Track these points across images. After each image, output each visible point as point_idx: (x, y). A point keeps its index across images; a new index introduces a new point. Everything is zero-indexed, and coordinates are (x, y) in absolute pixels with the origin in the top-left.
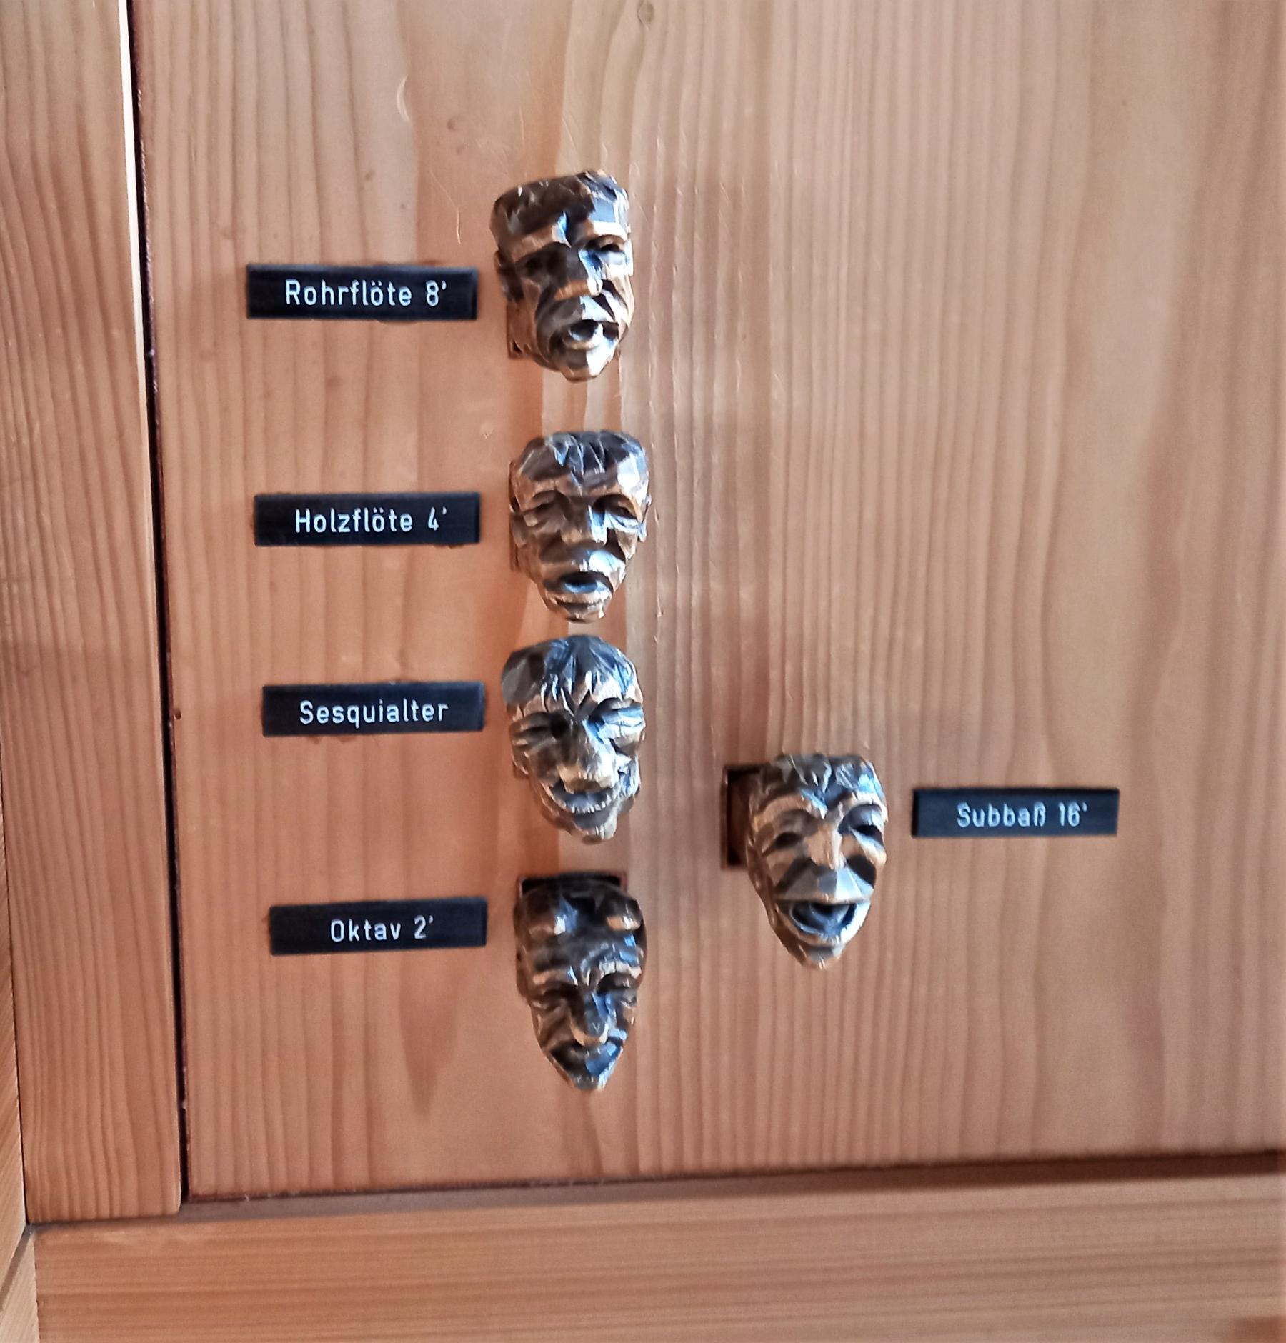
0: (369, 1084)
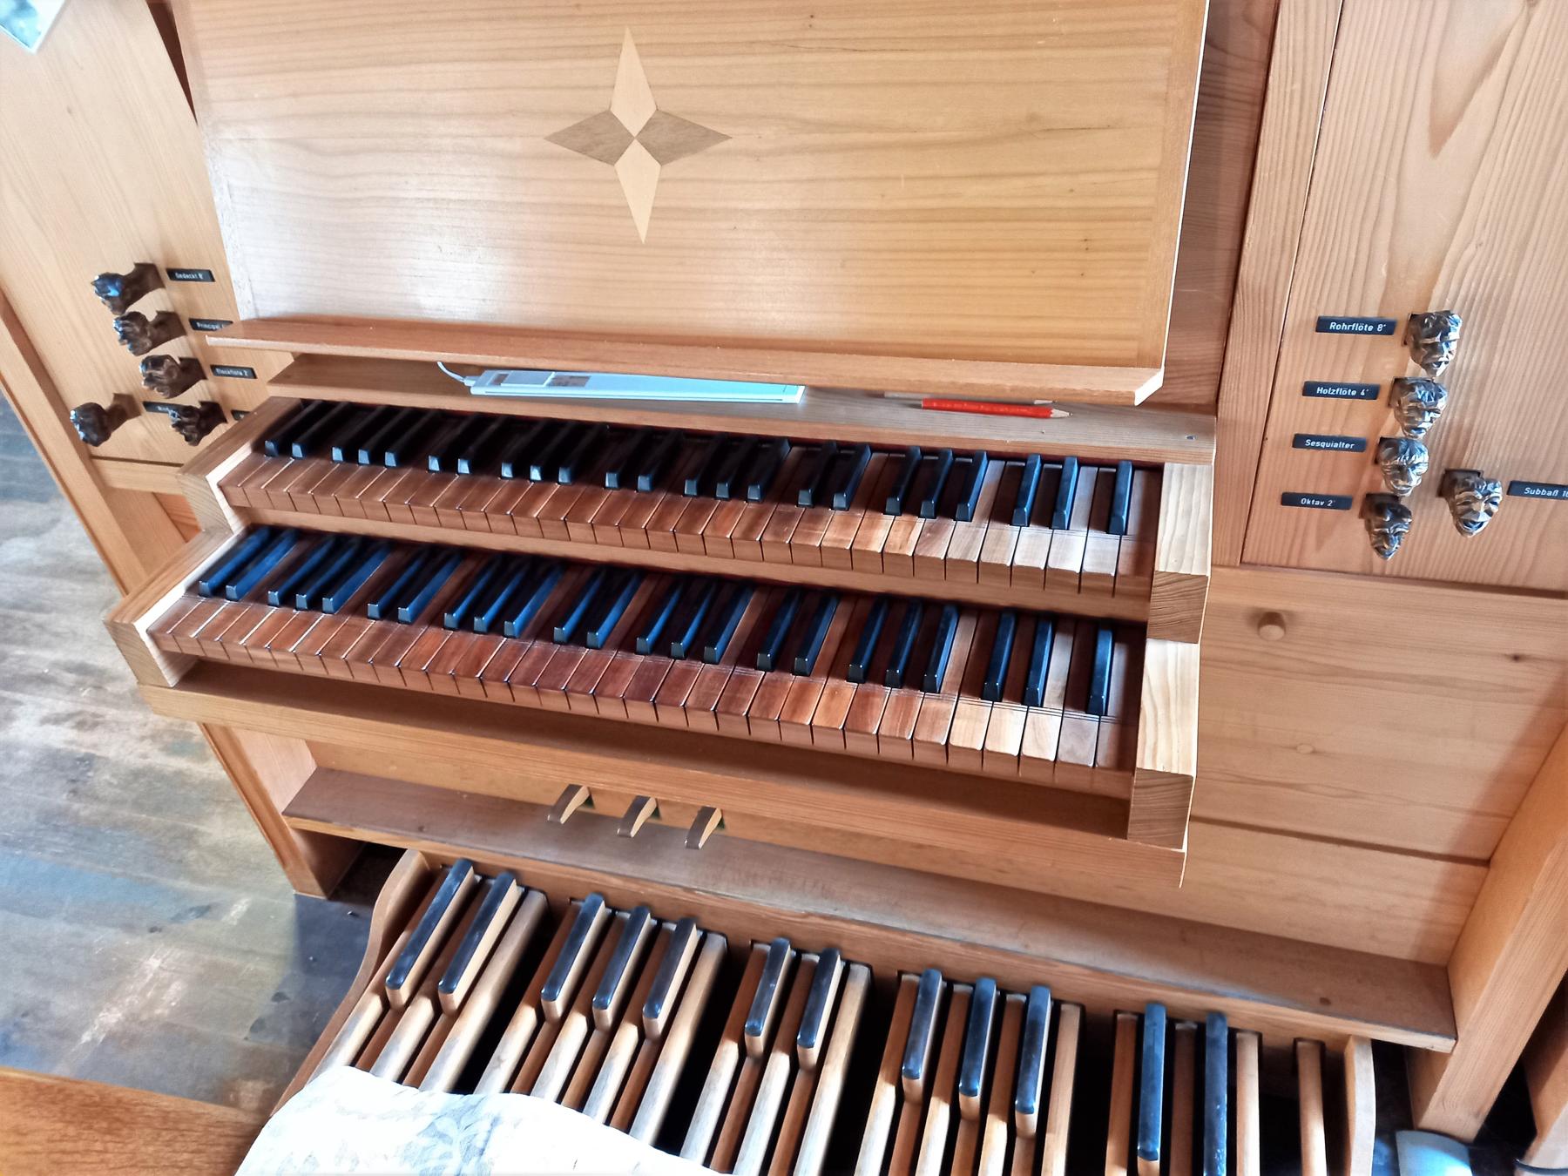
0: (1303, 541)
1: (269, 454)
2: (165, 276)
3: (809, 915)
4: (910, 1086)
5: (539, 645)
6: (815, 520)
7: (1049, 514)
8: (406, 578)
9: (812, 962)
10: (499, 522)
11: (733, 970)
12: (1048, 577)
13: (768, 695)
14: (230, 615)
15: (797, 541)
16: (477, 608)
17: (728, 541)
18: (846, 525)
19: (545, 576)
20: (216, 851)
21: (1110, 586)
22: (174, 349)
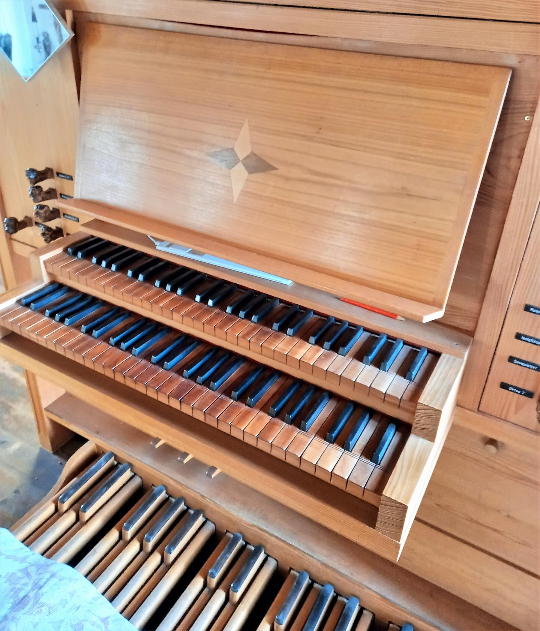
1: (69, 254)
2: (55, 175)
3: (253, 526)
4: (277, 627)
5: (144, 362)
6: (277, 337)
7: (379, 362)
8: (101, 317)
9: (251, 550)
10: (146, 304)
11: (214, 541)
12: (371, 391)
13: (232, 410)
14: (28, 315)
15: (265, 345)
16: (124, 339)
17: (237, 336)
18: (289, 343)
19: (159, 332)
20: (16, 419)
21: (398, 404)
22: (51, 204)
